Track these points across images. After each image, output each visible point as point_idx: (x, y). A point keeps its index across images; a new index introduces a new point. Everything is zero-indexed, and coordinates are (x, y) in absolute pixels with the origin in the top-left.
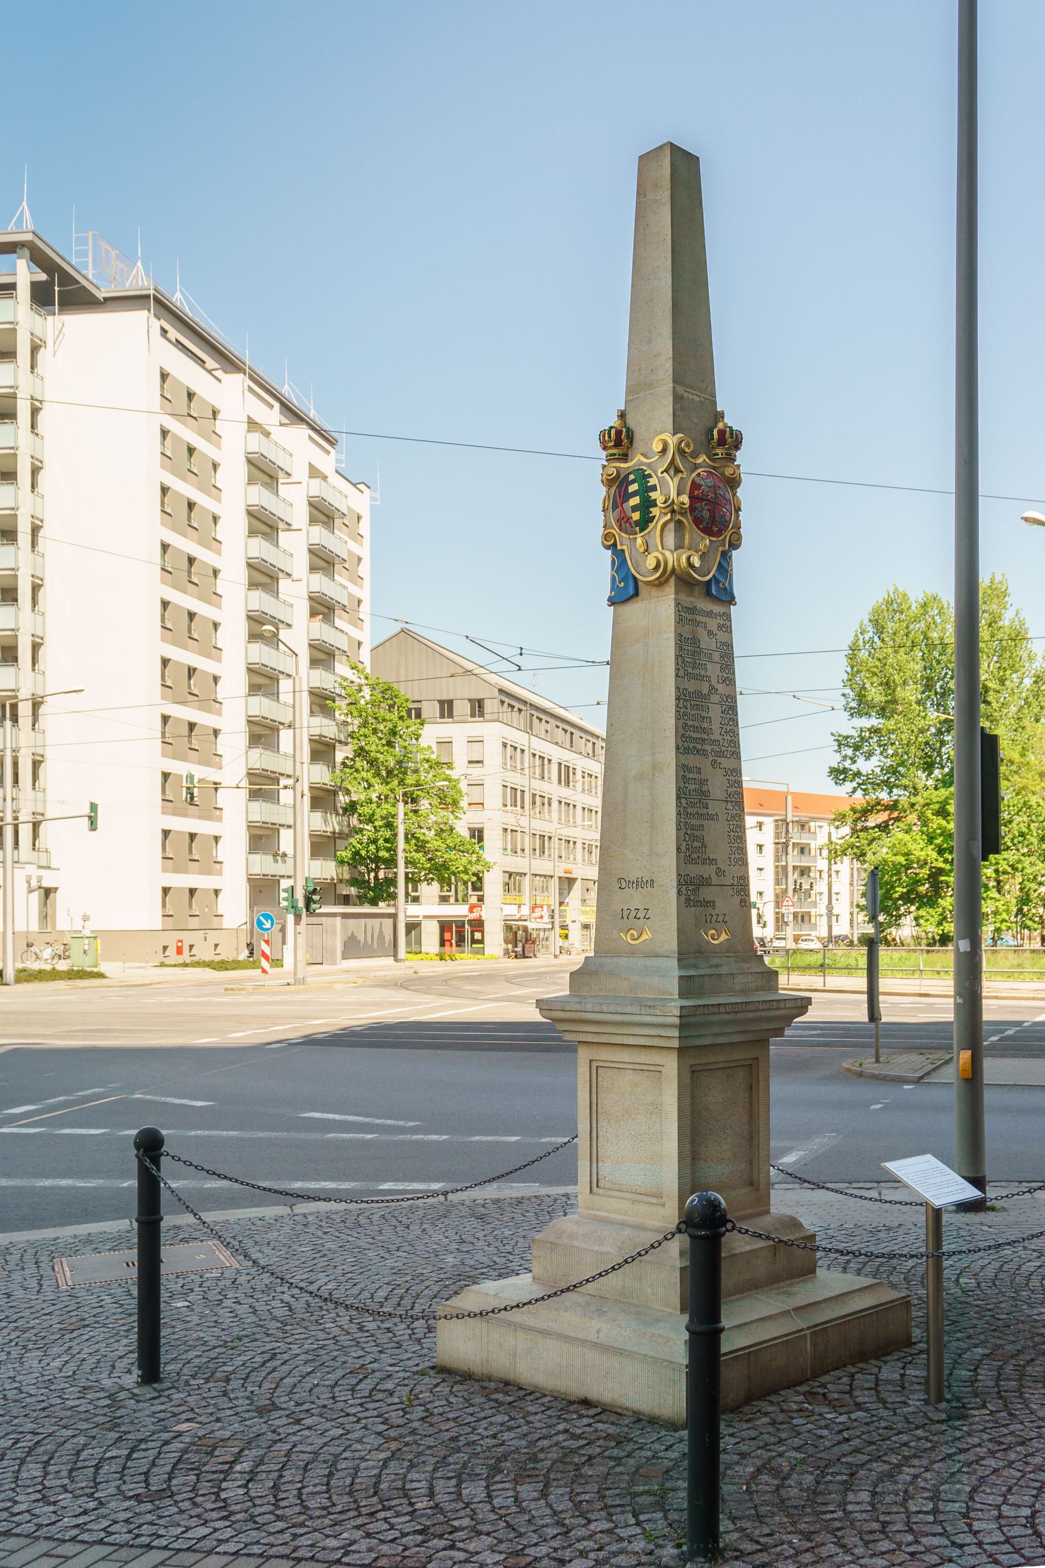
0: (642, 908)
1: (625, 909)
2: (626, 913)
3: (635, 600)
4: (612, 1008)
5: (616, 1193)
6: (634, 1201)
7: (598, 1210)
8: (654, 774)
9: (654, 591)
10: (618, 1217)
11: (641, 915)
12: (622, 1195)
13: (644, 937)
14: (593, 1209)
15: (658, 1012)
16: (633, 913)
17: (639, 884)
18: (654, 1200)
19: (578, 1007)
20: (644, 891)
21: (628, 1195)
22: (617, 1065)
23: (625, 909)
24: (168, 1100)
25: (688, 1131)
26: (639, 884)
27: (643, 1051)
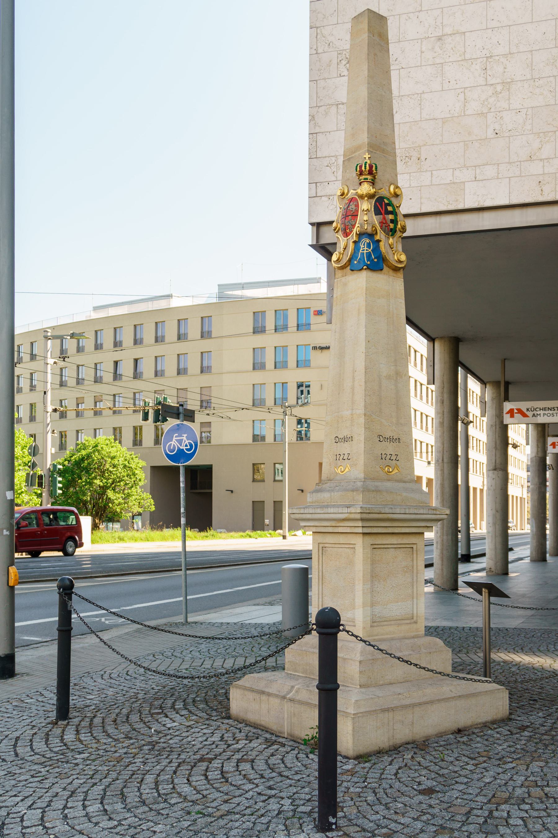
0: (393, 454)
1: (338, 454)
2: (384, 456)
3: (380, 272)
4: (411, 512)
5: (386, 623)
6: (399, 625)
7: (376, 635)
8: (396, 378)
9: (391, 272)
10: (389, 636)
11: (393, 458)
12: (389, 623)
13: (347, 470)
14: (372, 636)
15: (438, 513)
16: (389, 457)
17: (391, 440)
18: (408, 622)
19: (391, 511)
20: (395, 444)
21: (393, 622)
22: (386, 546)
23: (383, 454)
24: (124, 608)
25: (240, 604)
26: (391, 440)
27: (405, 536)
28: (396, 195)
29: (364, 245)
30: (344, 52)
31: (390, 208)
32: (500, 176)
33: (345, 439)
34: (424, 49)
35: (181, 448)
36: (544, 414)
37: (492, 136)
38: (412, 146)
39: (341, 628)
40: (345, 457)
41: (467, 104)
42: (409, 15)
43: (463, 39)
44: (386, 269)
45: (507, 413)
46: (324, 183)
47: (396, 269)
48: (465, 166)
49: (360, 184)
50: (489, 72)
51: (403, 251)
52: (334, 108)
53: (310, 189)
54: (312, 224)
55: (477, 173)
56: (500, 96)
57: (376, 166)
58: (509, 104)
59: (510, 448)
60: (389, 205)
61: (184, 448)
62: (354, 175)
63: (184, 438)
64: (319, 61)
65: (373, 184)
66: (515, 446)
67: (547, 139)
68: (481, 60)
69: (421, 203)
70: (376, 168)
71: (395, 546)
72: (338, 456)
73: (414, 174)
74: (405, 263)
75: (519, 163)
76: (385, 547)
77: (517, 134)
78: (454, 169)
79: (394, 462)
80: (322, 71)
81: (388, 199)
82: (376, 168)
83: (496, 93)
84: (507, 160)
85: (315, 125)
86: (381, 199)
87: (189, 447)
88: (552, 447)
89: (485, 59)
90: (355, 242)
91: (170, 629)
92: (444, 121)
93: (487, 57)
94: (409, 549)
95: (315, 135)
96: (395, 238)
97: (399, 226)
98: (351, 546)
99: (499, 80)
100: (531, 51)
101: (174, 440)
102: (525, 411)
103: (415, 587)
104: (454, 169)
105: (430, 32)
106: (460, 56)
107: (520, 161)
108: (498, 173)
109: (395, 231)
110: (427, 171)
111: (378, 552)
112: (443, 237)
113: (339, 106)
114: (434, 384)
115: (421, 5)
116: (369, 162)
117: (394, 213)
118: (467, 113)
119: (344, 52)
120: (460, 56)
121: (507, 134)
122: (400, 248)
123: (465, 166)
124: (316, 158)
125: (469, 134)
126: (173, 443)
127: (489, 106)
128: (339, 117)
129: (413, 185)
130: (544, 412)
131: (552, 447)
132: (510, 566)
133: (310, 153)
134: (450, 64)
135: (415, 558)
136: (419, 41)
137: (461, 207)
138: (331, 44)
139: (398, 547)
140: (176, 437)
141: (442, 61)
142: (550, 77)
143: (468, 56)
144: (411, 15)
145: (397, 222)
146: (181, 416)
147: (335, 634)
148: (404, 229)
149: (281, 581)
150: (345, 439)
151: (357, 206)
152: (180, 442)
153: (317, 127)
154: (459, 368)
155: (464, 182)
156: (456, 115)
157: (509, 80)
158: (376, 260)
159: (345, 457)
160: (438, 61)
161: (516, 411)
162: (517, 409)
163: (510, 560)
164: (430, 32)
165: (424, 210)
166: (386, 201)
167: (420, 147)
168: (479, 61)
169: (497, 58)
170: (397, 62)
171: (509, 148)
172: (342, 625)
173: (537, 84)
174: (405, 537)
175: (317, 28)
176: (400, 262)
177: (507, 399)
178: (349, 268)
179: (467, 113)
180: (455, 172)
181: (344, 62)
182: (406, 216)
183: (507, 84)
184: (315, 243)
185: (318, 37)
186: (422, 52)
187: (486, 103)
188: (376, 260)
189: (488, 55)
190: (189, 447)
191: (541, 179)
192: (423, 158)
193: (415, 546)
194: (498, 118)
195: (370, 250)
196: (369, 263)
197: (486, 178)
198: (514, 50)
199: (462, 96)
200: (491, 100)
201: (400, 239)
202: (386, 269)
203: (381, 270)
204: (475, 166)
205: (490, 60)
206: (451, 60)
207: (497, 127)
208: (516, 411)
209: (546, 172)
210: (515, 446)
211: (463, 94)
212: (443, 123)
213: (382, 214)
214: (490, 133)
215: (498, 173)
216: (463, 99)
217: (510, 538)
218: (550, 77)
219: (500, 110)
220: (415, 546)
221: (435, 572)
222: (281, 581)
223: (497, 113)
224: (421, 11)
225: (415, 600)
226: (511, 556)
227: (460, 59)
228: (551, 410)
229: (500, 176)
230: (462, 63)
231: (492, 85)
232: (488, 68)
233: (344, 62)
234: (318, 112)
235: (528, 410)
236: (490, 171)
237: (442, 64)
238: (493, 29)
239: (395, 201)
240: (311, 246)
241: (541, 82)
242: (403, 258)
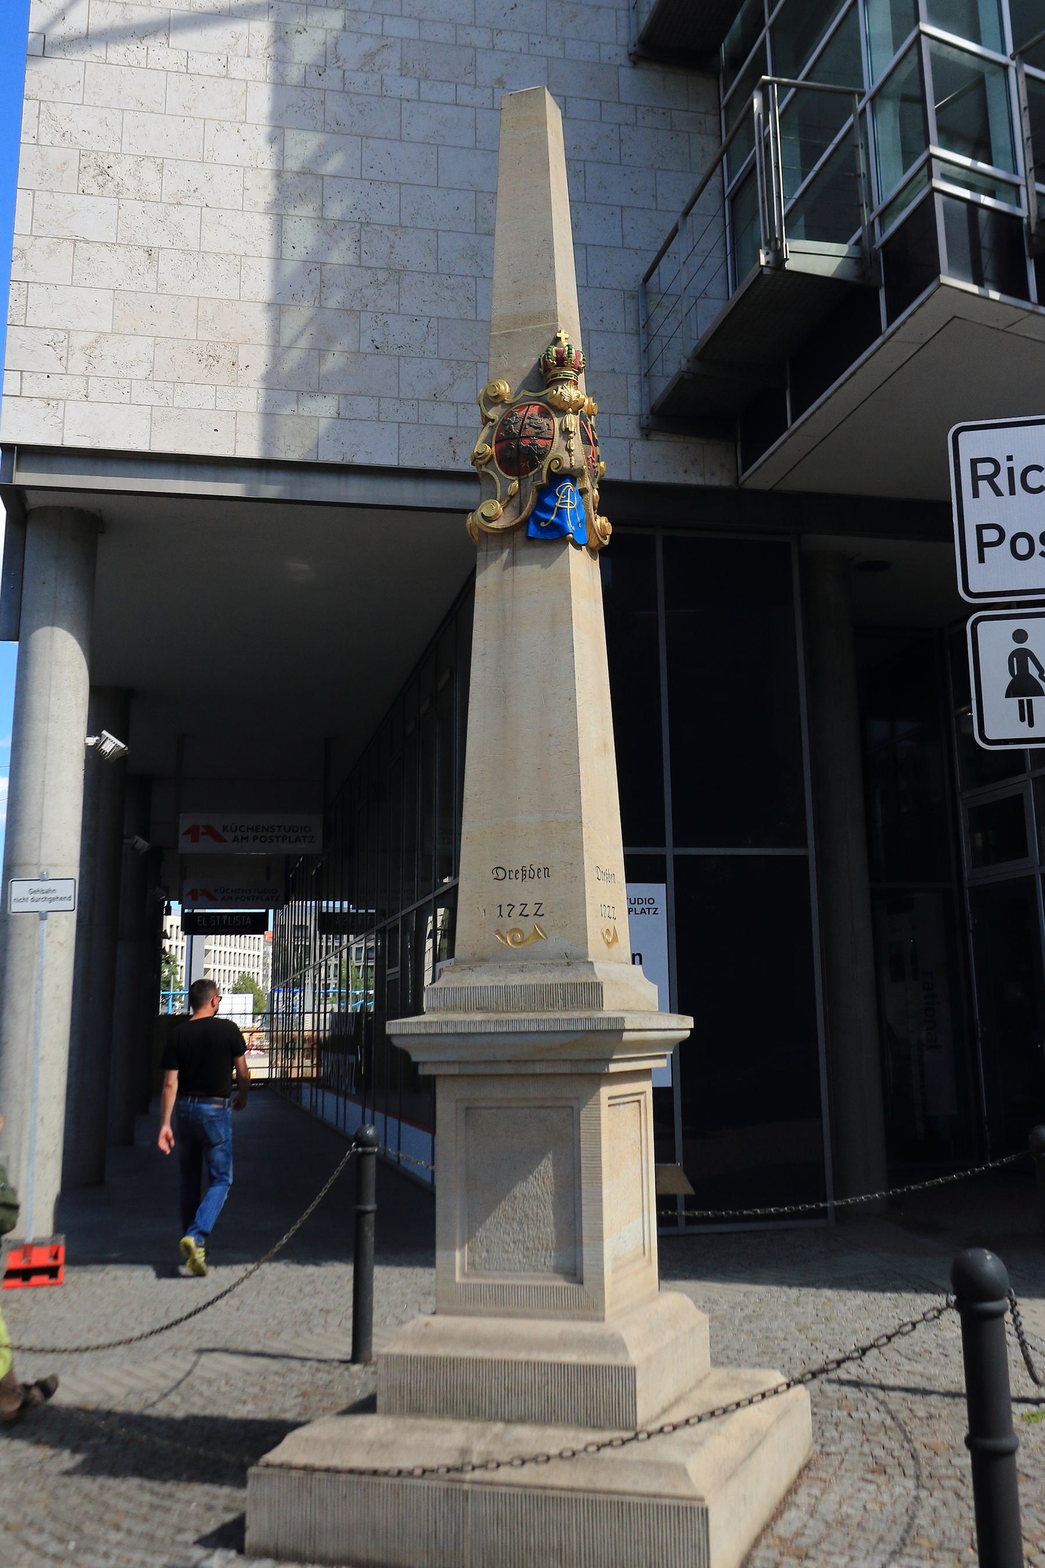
11: (530, 910)
16: (518, 910)
30: (93, 155)
32: (382, 417)
34: (248, 185)
36: (255, 838)
37: (368, 351)
38: (222, 340)
42: (223, 123)
43: (320, 185)
45: (185, 833)
46: (39, 375)
52: (68, 246)
56: (383, 288)
58: (399, 305)
67: (462, 372)
69: (236, 441)
75: (414, 402)
77: (412, 354)
80: (45, 178)
83: (374, 283)
88: (190, 897)
89: (358, 226)
93: (361, 223)
99: (381, 264)
100: (437, 231)
102: (219, 830)
107: (418, 400)
108: (380, 413)
112: (327, 508)
113: (78, 244)
119: (93, 155)
121: (396, 352)
128: (77, 262)
130: (255, 834)
131: (190, 897)
134: (297, 219)
138: (67, 135)
142: (467, 276)
144: (227, 125)
153: (29, 272)
157: (398, 267)
161: (202, 830)
162: (204, 827)
181: (92, 171)
187: (359, 295)
191: (452, 433)
192: (242, 364)
194: (381, 323)
200: (368, 292)
205: (366, 228)
208: (202, 830)
209: (461, 423)
211: (318, 272)
215: (380, 413)
216: (318, 281)
218: (467, 276)
219: (383, 310)
223: (379, 315)
228: (267, 830)
231: (370, 268)
233: (92, 171)
234: (33, 245)
235: (225, 829)
238: (372, 182)
241: (452, 281)
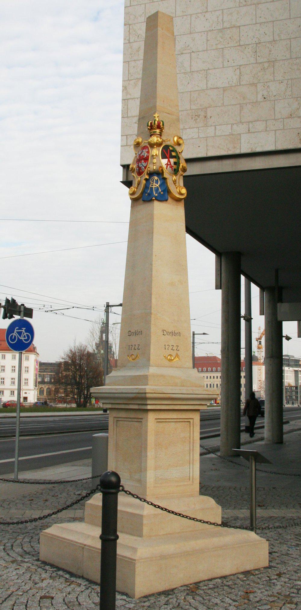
0: (175, 345)
2: (167, 347)
3: (165, 202)
9: (175, 202)
11: (175, 348)
16: (171, 347)
17: (173, 334)
20: (176, 337)
26: (173, 334)
28: (179, 144)
29: (153, 181)
31: (174, 154)
33: (136, 333)
34: (209, 39)
35: (21, 338)
37: (262, 100)
39: (121, 488)
40: (136, 348)
41: (242, 77)
42: (198, 15)
44: (170, 200)
47: (178, 200)
48: (241, 122)
49: (151, 136)
50: (258, 54)
51: (184, 186)
53: (122, 140)
54: (122, 166)
55: (250, 127)
57: (163, 122)
59: (284, 339)
60: (173, 151)
61: (23, 339)
62: (147, 129)
63: (23, 331)
64: (131, 48)
65: (161, 136)
66: (288, 338)
68: (252, 45)
69: (207, 150)
70: (163, 124)
71: (175, 420)
72: (131, 347)
73: (202, 128)
74: (186, 195)
76: (165, 421)
77: (280, 98)
78: (232, 124)
79: (175, 351)
81: (172, 147)
82: (163, 124)
83: (264, 69)
84: (273, 117)
85: (127, 93)
86: (166, 147)
87: (26, 338)
90: (146, 180)
91: (53, 485)
92: (224, 89)
93: (257, 44)
94: (187, 423)
95: (126, 101)
96: (178, 176)
97: (181, 167)
98: (139, 420)
99: (265, 60)
101: (15, 332)
103: (191, 454)
104: (232, 124)
105: (213, 27)
106: (236, 43)
107: (283, 119)
109: (178, 171)
110: (211, 126)
111: (161, 425)
114: (221, 289)
115: (207, 8)
116: (157, 119)
117: (177, 157)
118: (242, 83)
120: (236, 43)
121: (273, 98)
122: (182, 183)
123: (241, 122)
124: (127, 117)
125: (244, 98)
126: (14, 334)
127: (259, 78)
129: (201, 136)
132: (284, 436)
133: (122, 114)
134: (229, 49)
135: (192, 431)
136: (206, 33)
137: (237, 152)
139: (177, 420)
140: (17, 329)
141: (223, 47)
143: (242, 43)
144: (199, 15)
145: (179, 164)
146: (22, 313)
147: (116, 494)
148: (184, 170)
149: (91, 447)
150: (136, 333)
151: (148, 152)
152: (20, 334)
154: (242, 276)
155: (240, 134)
156: (234, 85)
157: (273, 60)
158: (162, 193)
159: (136, 348)
160: (219, 47)
163: (284, 431)
164: (213, 27)
165: (211, 154)
166: (171, 149)
167: (206, 108)
168: (250, 46)
169: (264, 44)
170: (189, 48)
171: (274, 108)
172: (122, 486)
173: (295, 62)
174: (184, 413)
175: (130, 25)
176: (181, 194)
177: (281, 300)
178: (141, 199)
179: (242, 83)
180: (233, 126)
182: (188, 161)
183: (272, 63)
184: (125, 180)
185: (131, 31)
186: (207, 40)
188: (162, 193)
189: (257, 42)
190: (26, 338)
192: (209, 117)
193: (191, 421)
194: (266, 87)
195: (158, 185)
196: (157, 195)
197: (256, 131)
198: (277, 38)
199: (238, 72)
201: (182, 177)
202: (170, 200)
203: (166, 200)
204: (249, 122)
206: (229, 45)
207: (265, 94)
210: (288, 338)
211: (238, 70)
212: (224, 91)
213: (167, 158)
214: (260, 98)
216: (239, 73)
217: (284, 413)
220: (191, 421)
221: (221, 441)
222: (91, 447)
224: (207, 12)
225: (191, 465)
226: (286, 428)
227: (236, 45)
229: (268, 129)
230: (238, 48)
231: (261, 63)
232: (258, 51)
236: (260, 126)
237: (223, 48)
239: (178, 149)
240: (121, 182)
242: (184, 191)
